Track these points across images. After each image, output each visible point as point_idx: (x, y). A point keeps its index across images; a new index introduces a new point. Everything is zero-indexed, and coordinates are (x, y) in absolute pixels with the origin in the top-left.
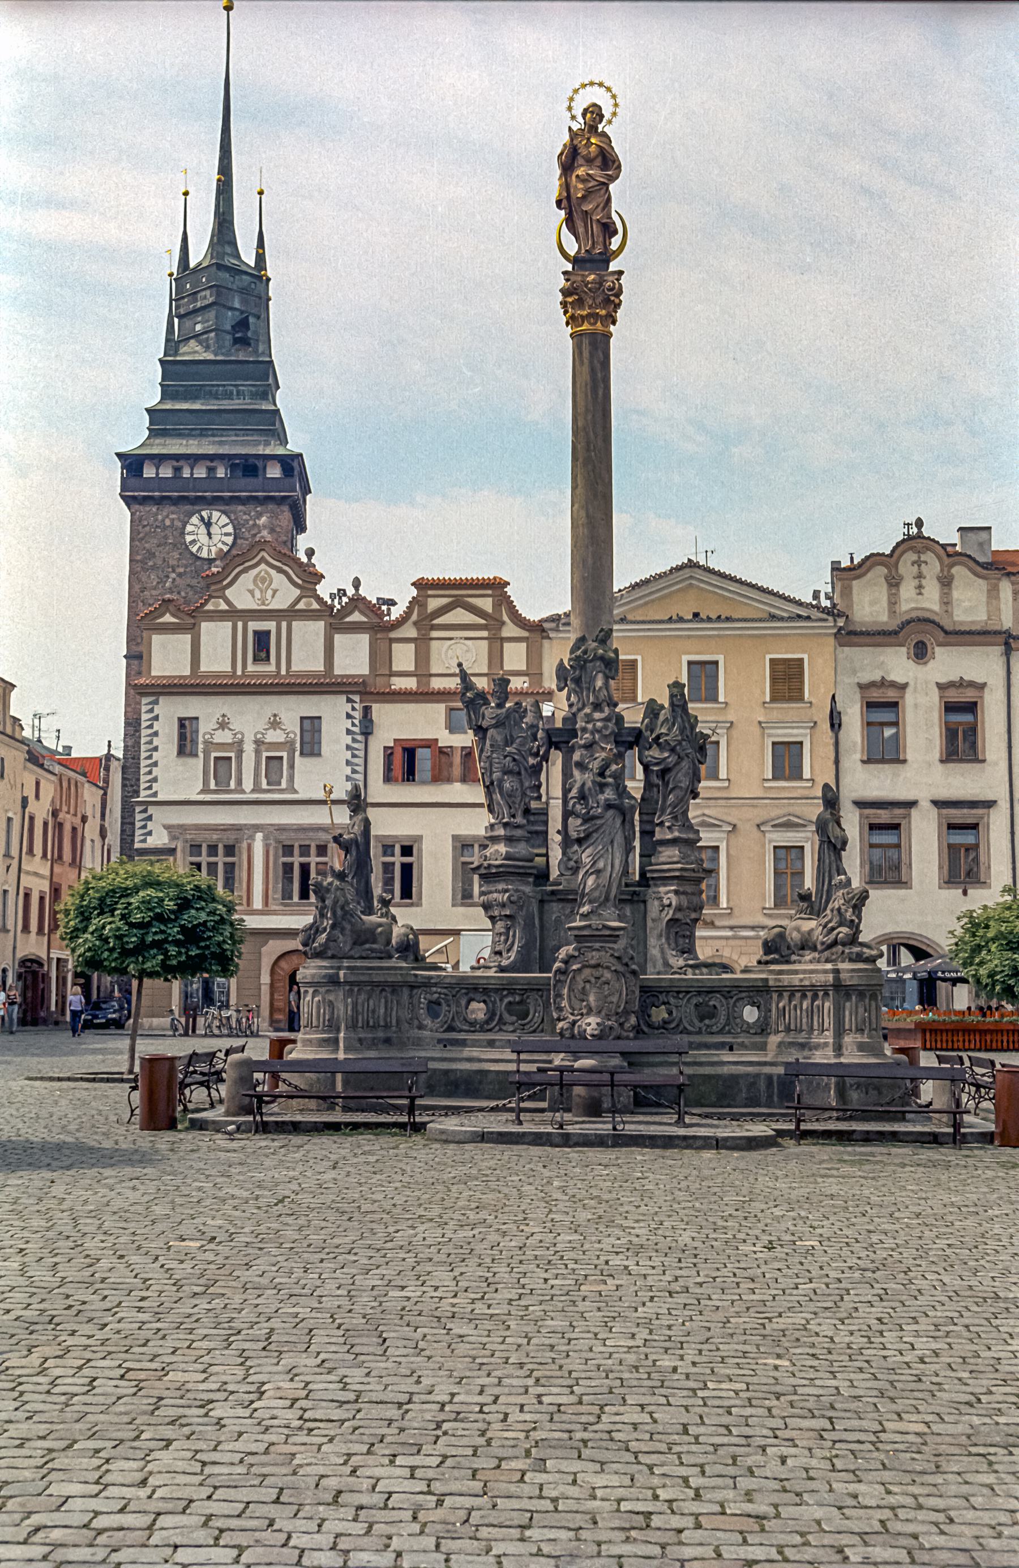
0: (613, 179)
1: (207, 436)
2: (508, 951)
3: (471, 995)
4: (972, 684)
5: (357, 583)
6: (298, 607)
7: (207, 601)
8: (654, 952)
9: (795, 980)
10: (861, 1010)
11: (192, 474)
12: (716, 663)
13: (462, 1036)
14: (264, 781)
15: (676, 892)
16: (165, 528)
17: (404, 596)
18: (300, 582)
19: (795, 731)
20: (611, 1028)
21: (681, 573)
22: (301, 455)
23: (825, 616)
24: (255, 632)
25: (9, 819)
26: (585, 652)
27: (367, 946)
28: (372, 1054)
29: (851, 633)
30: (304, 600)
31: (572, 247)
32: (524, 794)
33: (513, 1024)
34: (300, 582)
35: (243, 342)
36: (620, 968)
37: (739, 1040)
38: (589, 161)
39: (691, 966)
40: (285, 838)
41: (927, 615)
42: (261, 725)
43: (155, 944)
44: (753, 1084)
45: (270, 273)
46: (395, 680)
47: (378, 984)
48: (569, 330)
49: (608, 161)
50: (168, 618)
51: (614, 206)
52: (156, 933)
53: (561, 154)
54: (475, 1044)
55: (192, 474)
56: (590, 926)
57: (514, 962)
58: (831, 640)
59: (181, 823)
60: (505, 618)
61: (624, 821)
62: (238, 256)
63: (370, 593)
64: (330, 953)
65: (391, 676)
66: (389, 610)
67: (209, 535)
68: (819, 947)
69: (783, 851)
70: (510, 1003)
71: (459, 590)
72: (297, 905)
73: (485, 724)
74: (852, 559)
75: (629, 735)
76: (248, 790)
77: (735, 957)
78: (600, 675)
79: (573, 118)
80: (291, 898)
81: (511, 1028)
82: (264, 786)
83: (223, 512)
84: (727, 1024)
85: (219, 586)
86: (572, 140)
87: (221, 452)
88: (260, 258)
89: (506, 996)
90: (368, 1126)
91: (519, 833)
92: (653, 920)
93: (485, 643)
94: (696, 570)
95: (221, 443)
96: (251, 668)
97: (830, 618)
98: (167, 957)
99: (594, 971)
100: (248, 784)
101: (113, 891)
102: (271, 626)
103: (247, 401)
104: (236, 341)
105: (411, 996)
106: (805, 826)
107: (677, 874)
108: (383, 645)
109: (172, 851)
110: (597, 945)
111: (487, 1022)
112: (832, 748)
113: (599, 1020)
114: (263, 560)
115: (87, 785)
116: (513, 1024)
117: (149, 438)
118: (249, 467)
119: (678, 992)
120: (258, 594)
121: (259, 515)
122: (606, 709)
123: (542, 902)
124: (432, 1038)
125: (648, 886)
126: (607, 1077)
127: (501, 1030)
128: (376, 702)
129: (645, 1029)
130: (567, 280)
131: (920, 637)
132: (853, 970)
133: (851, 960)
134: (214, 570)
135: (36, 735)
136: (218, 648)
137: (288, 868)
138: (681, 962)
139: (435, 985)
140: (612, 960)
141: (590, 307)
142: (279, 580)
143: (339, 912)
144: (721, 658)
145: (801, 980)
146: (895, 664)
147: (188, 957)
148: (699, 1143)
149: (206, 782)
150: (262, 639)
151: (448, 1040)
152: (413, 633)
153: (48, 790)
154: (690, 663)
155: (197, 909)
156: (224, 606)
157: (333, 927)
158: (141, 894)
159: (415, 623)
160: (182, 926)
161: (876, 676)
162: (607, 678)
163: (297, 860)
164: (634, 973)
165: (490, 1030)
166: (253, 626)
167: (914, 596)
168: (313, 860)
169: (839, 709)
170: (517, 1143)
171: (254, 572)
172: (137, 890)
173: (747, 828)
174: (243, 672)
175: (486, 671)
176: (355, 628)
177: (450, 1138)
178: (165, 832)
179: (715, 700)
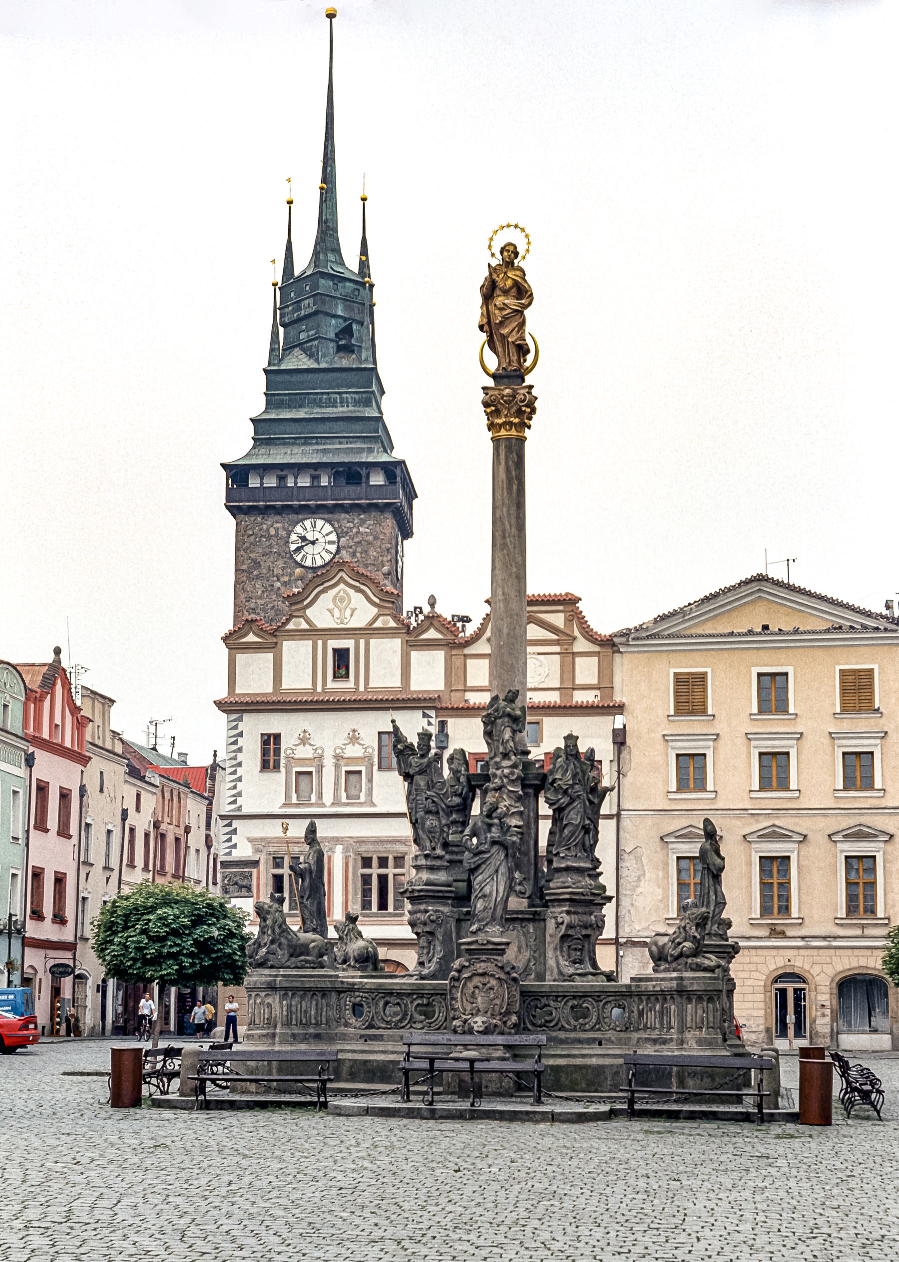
1: (311, 444)
2: (430, 961)
3: (388, 999)
5: (432, 602)
6: (375, 625)
7: (288, 621)
8: (551, 962)
10: (700, 1012)
11: (296, 483)
12: (786, 674)
14: (344, 795)
15: (568, 913)
16: (269, 537)
18: (377, 601)
19: (865, 742)
20: (496, 1026)
21: (750, 586)
22: (404, 462)
24: (335, 651)
25: (109, 832)
26: (497, 710)
27: (302, 958)
28: (303, 1047)
30: (381, 618)
31: (492, 362)
32: (442, 831)
33: (422, 1022)
34: (377, 601)
35: (347, 349)
36: (503, 976)
37: (607, 1036)
38: (506, 292)
39: (579, 975)
40: (366, 850)
42: (341, 740)
43: (170, 956)
44: (617, 1073)
45: (374, 279)
46: (469, 696)
47: (309, 989)
48: (490, 434)
49: (522, 292)
50: (251, 638)
51: (528, 328)
52: (171, 946)
53: (483, 286)
54: (391, 1038)
55: (296, 483)
56: (476, 941)
57: (435, 971)
59: (263, 835)
60: (577, 633)
61: (507, 856)
62: (342, 264)
63: (445, 610)
64: (269, 963)
65: (465, 691)
66: (463, 626)
67: (318, 539)
68: (669, 958)
70: (418, 1005)
72: (376, 915)
73: (411, 771)
75: (536, 778)
76: (328, 803)
77: (807, 967)
78: (508, 729)
79: (493, 255)
80: (370, 909)
81: (420, 1026)
82: (344, 799)
83: (329, 521)
84: (598, 1022)
85: (299, 606)
86: (491, 274)
87: (325, 460)
88: (364, 266)
89: (415, 999)
90: (288, 1104)
91: (438, 863)
92: (551, 936)
93: (558, 657)
94: (764, 583)
95: (325, 451)
96: (331, 684)
98: (182, 968)
99: (481, 979)
100: (328, 798)
101: (136, 909)
102: (348, 643)
103: (351, 408)
104: (340, 349)
105: (339, 1000)
106: (876, 836)
107: (567, 896)
108: (458, 662)
109: (256, 863)
110: (484, 957)
111: (401, 1021)
113: (485, 1019)
114: (341, 580)
115: (190, 795)
116: (422, 1022)
117: (254, 447)
118: (351, 474)
119: (557, 997)
120: (337, 613)
121: (362, 522)
122: (513, 757)
123: (459, 921)
124: (355, 1034)
125: (548, 907)
126: (466, 1065)
127: (411, 1027)
128: (451, 716)
129: (530, 1027)
130: (487, 394)
132: (694, 978)
133: (692, 970)
134: (296, 590)
135: (152, 741)
136: (300, 664)
137: (366, 880)
138: (571, 971)
139: (358, 990)
141: (506, 416)
142: (357, 599)
143: (277, 930)
145: (654, 987)
147: (202, 966)
148: (538, 1117)
149: (287, 796)
150: (341, 656)
151: (368, 1035)
152: (487, 649)
153: (149, 802)
154: (760, 675)
155: (209, 925)
156: (304, 626)
157: (273, 942)
158: (159, 912)
159: (489, 640)
160: (195, 940)
162: (514, 732)
163: (375, 871)
164: (515, 980)
165: (403, 1027)
166: (334, 644)
168: (390, 871)
170: (394, 1116)
171: (332, 593)
172: (152, 909)
173: (818, 839)
174: (323, 689)
175: (558, 686)
176: (431, 645)
177: (343, 1112)
178: (249, 844)
179: (786, 711)
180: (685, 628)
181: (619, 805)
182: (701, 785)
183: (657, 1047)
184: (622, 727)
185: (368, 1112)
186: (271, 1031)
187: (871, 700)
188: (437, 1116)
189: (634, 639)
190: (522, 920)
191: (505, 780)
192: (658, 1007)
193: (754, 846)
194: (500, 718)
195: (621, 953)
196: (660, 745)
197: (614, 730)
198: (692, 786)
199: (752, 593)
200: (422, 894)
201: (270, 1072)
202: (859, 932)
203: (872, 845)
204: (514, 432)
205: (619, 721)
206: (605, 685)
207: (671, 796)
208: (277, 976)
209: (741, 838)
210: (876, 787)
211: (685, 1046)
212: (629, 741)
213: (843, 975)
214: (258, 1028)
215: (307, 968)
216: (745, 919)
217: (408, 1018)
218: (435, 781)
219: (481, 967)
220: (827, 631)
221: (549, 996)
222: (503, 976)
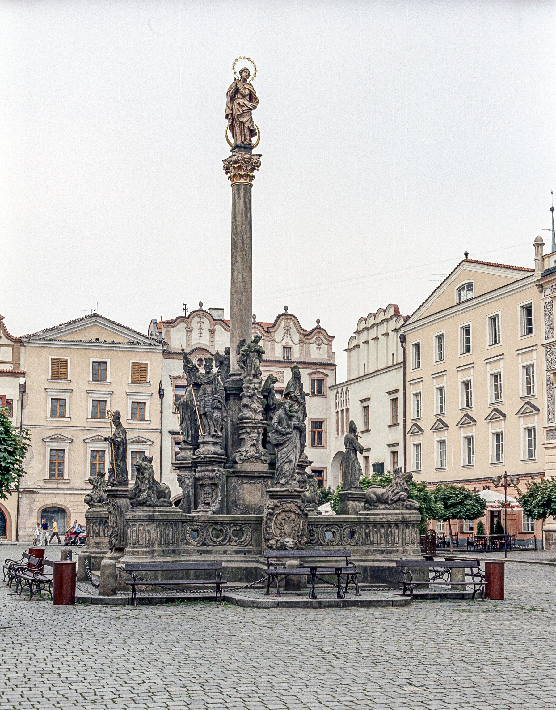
0: (255, 107)
2: (213, 502)
9: (378, 518)
12: (106, 363)
23: (158, 344)
27: (162, 499)
29: (169, 353)
36: (300, 513)
38: (244, 97)
41: (203, 347)
47: (168, 521)
49: (252, 97)
54: (217, 552)
56: (288, 490)
58: (160, 355)
68: (390, 502)
69: (135, 453)
70: (234, 530)
74: (161, 318)
79: (235, 73)
91: (218, 440)
97: (161, 345)
105: (182, 527)
106: (146, 442)
110: (289, 500)
111: (222, 541)
112: (160, 406)
116: (236, 541)
119: (317, 525)
127: (230, 545)
133: (407, 508)
139: (196, 521)
140: (296, 508)
143: (151, 481)
144: (108, 361)
145: (381, 519)
151: (202, 550)
157: (149, 488)
167: (198, 337)
169: (163, 388)
170: (295, 607)
173: (78, 442)
177: (259, 606)
179: (105, 381)
180: (58, 337)
181: (21, 422)
182: (63, 415)
183: (384, 555)
184: (23, 383)
185: (279, 605)
186: (151, 549)
187: (146, 378)
188: (322, 606)
189: (32, 340)
190: (264, 477)
191: (256, 391)
192: (383, 531)
193: (88, 445)
194: (252, 352)
195: (20, 496)
196: (44, 393)
197: (20, 385)
198: (58, 414)
199: (92, 322)
200: (212, 459)
201: (156, 578)
202: (55, 486)
203: (144, 446)
204: (248, 181)
205: (22, 380)
207: (48, 419)
208: (154, 511)
209: (82, 441)
210: (146, 419)
211: (405, 554)
212: (27, 391)
213: (62, 507)
214: (142, 547)
215: (165, 506)
216: (83, 481)
217: (228, 538)
218: (218, 389)
219: (287, 506)
220: (128, 343)
221: (312, 525)
222: (300, 513)
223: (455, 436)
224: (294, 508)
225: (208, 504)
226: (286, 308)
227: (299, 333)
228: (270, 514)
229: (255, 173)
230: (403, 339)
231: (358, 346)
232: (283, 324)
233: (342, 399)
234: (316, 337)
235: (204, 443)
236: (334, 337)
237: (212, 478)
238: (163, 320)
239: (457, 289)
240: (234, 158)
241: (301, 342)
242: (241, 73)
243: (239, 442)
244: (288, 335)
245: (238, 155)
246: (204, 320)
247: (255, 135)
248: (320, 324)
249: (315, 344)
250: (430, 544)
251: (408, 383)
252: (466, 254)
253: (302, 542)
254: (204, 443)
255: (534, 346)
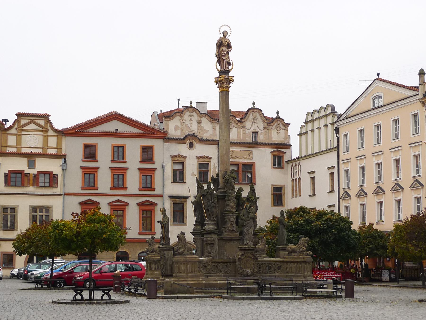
0: (230, 51)
4: (208, 158)
13: (212, 274)
17: (12, 119)
29: (168, 139)
38: (225, 46)
46: (8, 148)
49: (229, 46)
66: (6, 123)
71: (32, 117)
110: (249, 252)
131: (191, 141)
146: (182, 149)
159: (16, 129)
161: (177, 154)
206: (58, 147)
219: (248, 255)
223: (371, 201)
224: (251, 256)
225: (210, 253)
226: (254, 104)
227: (263, 121)
228: (239, 258)
229: (231, 85)
230: (337, 131)
231: (306, 133)
232: (251, 115)
233: (296, 171)
234: (276, 124)
235: (208, 224)
236: (290, 124)
237: (212, 241)
238: (162, 112)
239: (372, 98)
240: (220, 79)
241: (265, 128)
242: (223, 33)
243: (225, 223)
244: (256, 124)
245: (222, 77)
246: (194, 114)
247: (231, 65)
248: (279, 115)
249: (275, 130)
250: (50, 236)
251: (341, 162)
252: (378, 74)
253: (255, 271)
254: (208, 224)
255: (419, 142)
